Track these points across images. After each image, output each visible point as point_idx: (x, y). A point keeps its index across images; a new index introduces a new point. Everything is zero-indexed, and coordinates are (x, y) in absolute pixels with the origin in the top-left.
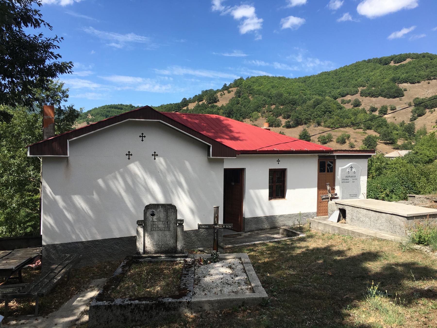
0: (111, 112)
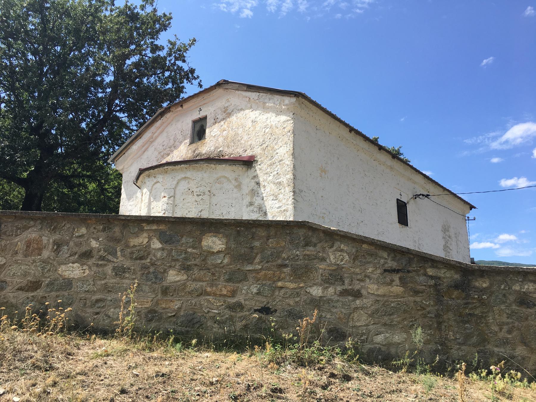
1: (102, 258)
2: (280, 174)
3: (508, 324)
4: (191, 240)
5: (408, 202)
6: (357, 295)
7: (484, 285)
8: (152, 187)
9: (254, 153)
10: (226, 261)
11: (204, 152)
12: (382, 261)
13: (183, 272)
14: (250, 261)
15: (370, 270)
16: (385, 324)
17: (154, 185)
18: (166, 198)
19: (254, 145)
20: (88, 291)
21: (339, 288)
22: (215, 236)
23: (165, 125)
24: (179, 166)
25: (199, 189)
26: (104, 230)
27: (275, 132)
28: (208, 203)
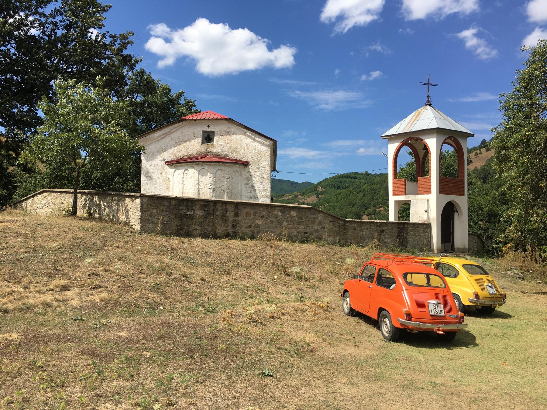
0: (342, 183)
6: (324, 228)
11: (214, 151)
23: (180, 127)
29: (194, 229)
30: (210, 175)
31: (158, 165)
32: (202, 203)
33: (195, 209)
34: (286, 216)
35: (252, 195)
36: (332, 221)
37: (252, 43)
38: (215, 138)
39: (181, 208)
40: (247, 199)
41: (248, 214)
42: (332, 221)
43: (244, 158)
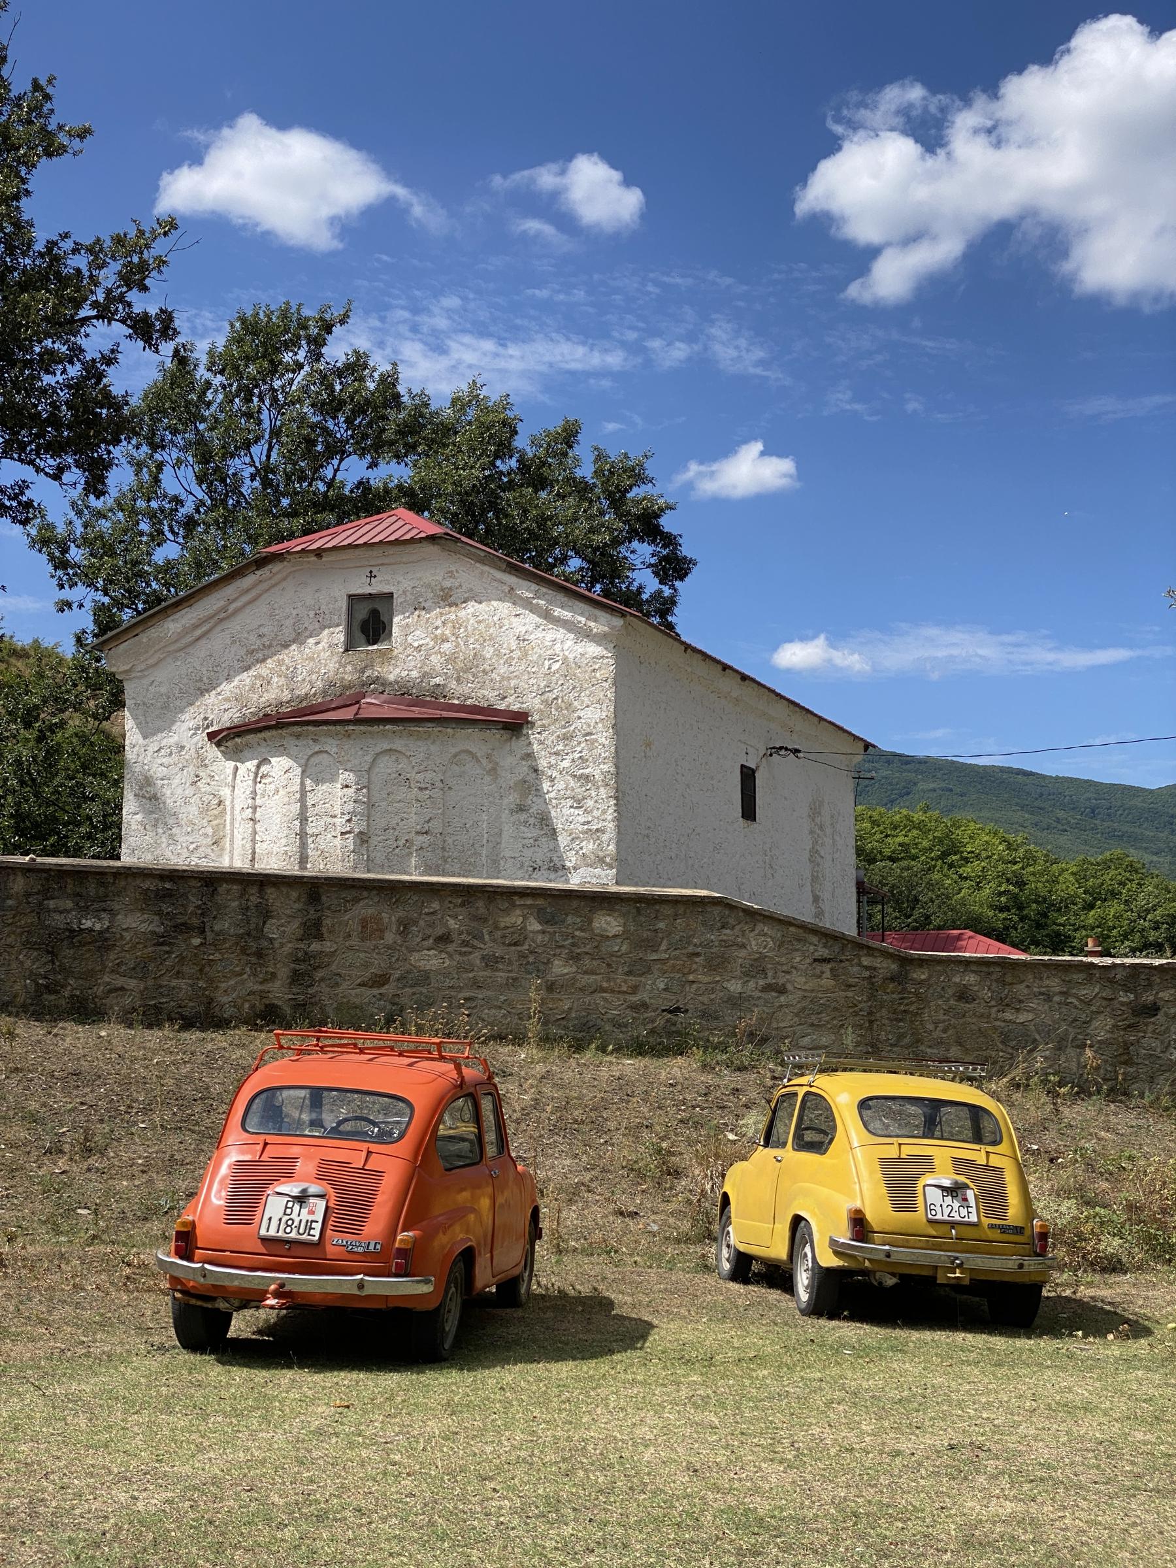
1: (465, 943)
2: (587, 760)
3: (944, 1021)
4: (579, 920)
5: (758, 767)
6: (782, 990)
7: (923, 977)
8: (308, 760)
9: (525, 706)
10: (624, 948)
11: (392, 678)
12: (812, 948)
13: (571, 962)
14: (655, 948)
15: (798, 959)
16: (812, 1025)
17: (311, 756)
18: (352, 790)
19: (524, 689)
20: (452, 987)
21: (761, 983)
22: (609, 915)
23: (265, 586)
24: (381, 727)
25: (422, 775)
26: (463, 905)
27: (574, 675)
28: (441, 806)
29: (110, 991)
30: (346, 776)
31: (183, 747)
32: (147, 884)
33: (117, 907)
34: (566, 936)
35: (540, 855)
36: (828, 961)
37: (948, 154)
38: (396, 620)
39: (52, 904)
40: (520, 873)
41: (370, 929)
42: (828, 961)
43: (510, 700)
